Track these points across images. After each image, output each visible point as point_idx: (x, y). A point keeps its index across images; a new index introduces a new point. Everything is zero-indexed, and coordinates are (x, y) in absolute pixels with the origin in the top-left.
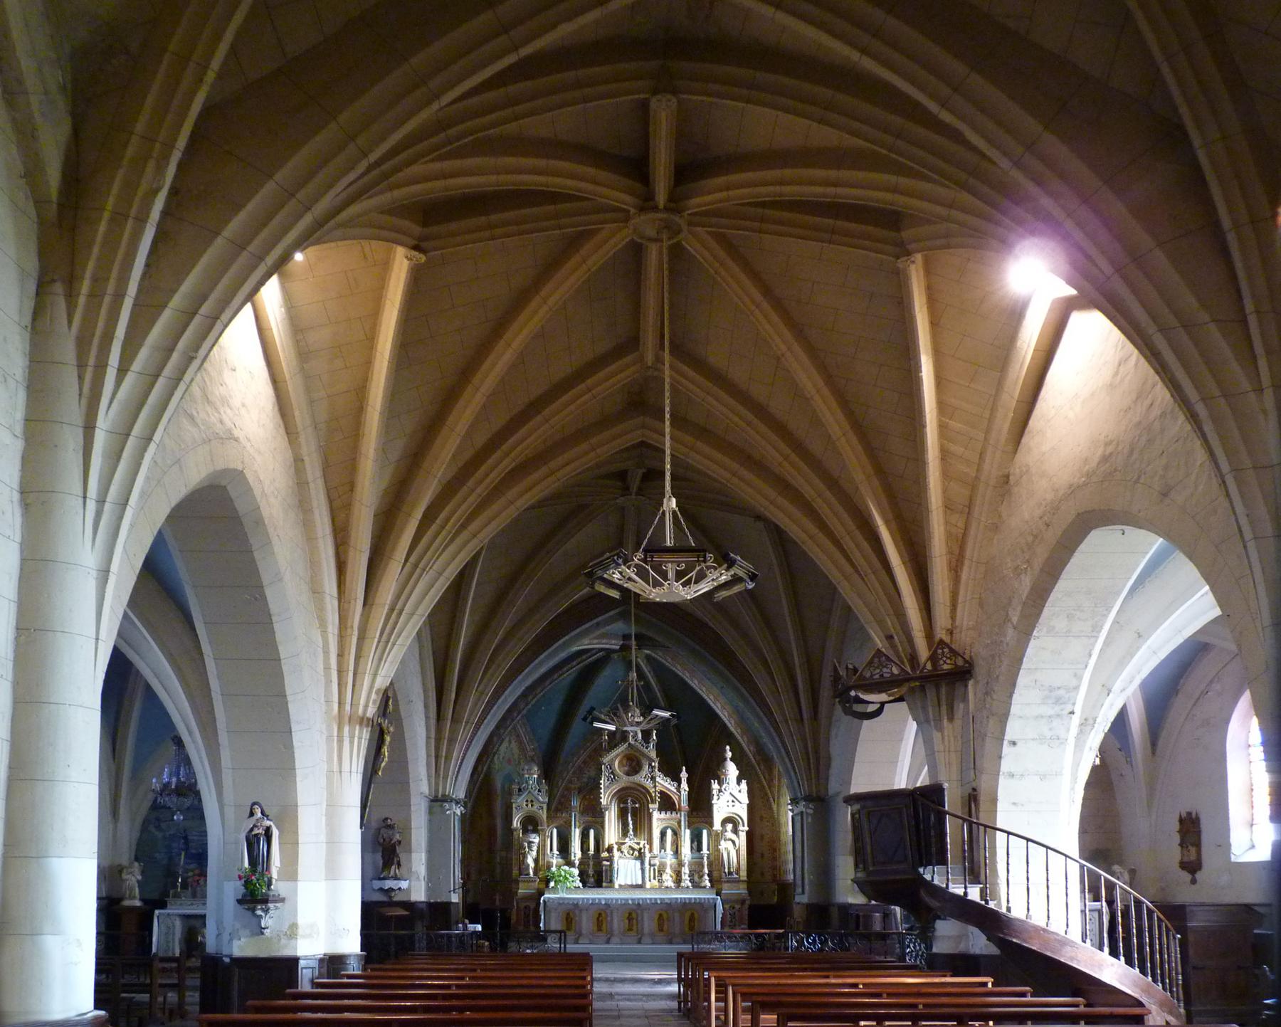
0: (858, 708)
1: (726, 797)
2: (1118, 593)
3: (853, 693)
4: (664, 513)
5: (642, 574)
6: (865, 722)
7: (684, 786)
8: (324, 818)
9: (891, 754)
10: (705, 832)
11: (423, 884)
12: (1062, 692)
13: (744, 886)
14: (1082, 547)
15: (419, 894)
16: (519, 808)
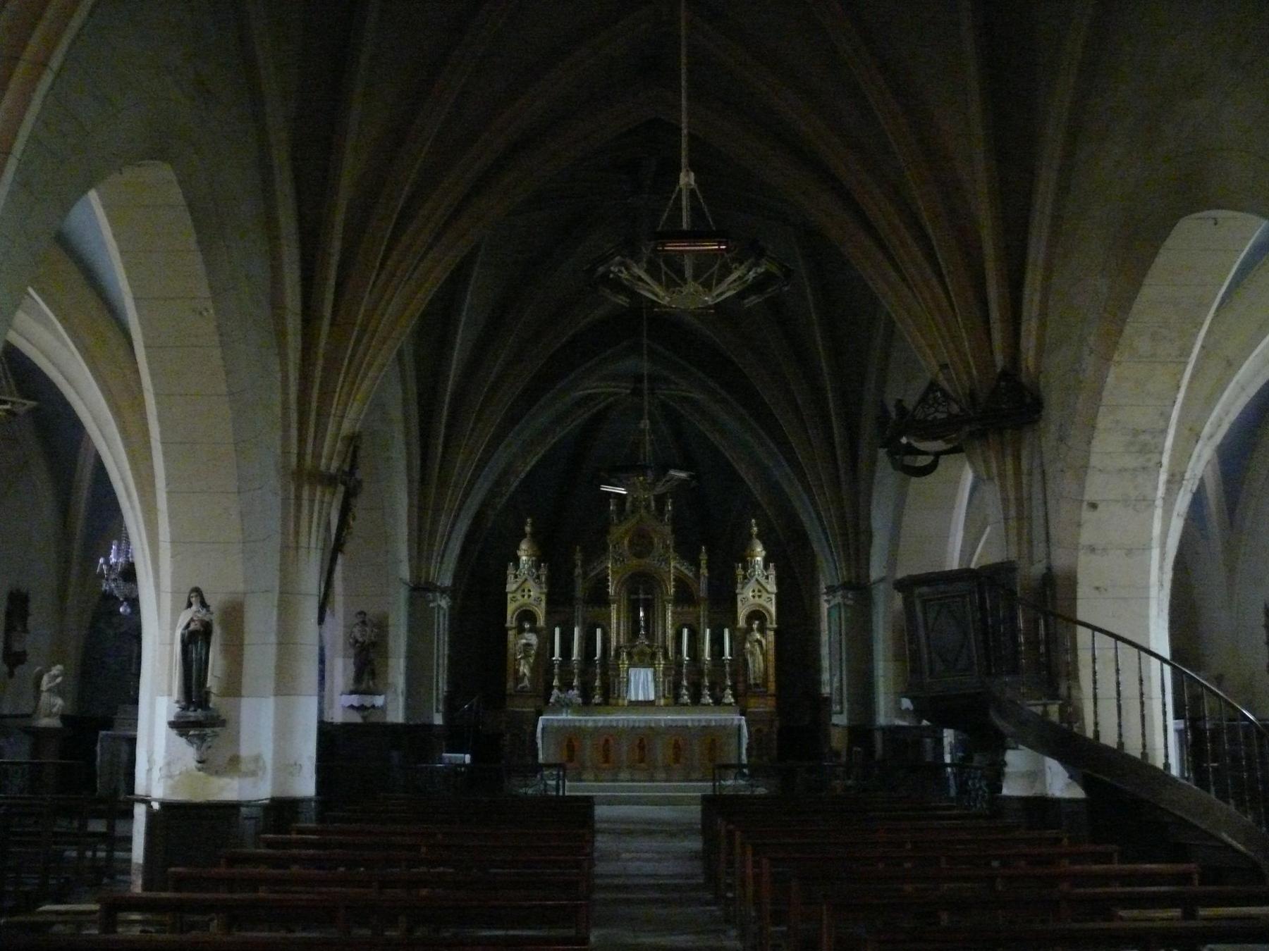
0: (908, 460)
1: (752, 585)
2: (1208, 307)
3: (904, 440)
4: (680, 190)
5: (653, 271)
6: (914, 479)
7: (704, 571)
8: (275, 612)
9: (949, 520)
10: (726, 632)
11: (401, 701)
12: (1147, 437)
13: (771, 702)
14: (1169, 242)
15: (397, 715)
16: (514, 600)
